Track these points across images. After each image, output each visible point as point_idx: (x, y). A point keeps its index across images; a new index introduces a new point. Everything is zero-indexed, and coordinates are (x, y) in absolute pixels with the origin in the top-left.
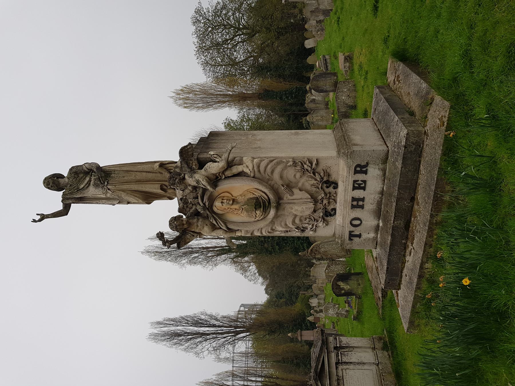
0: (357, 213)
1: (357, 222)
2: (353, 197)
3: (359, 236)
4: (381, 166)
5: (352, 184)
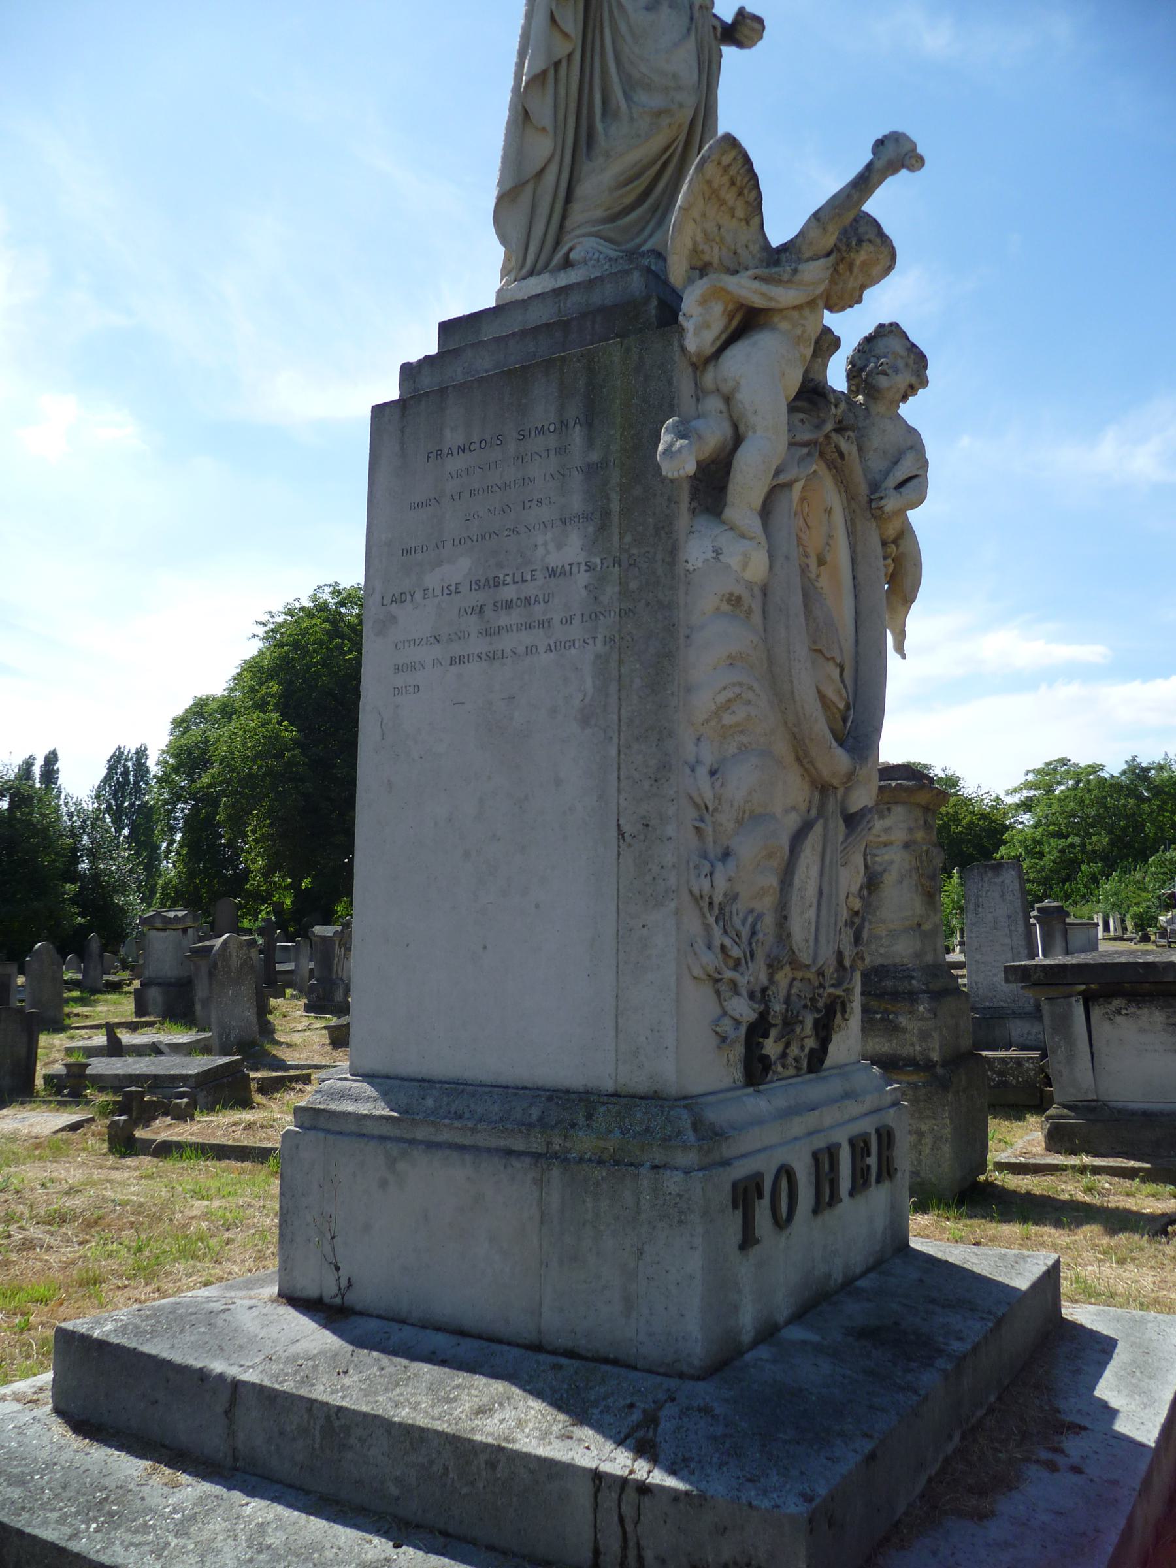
3: (748, 1241)
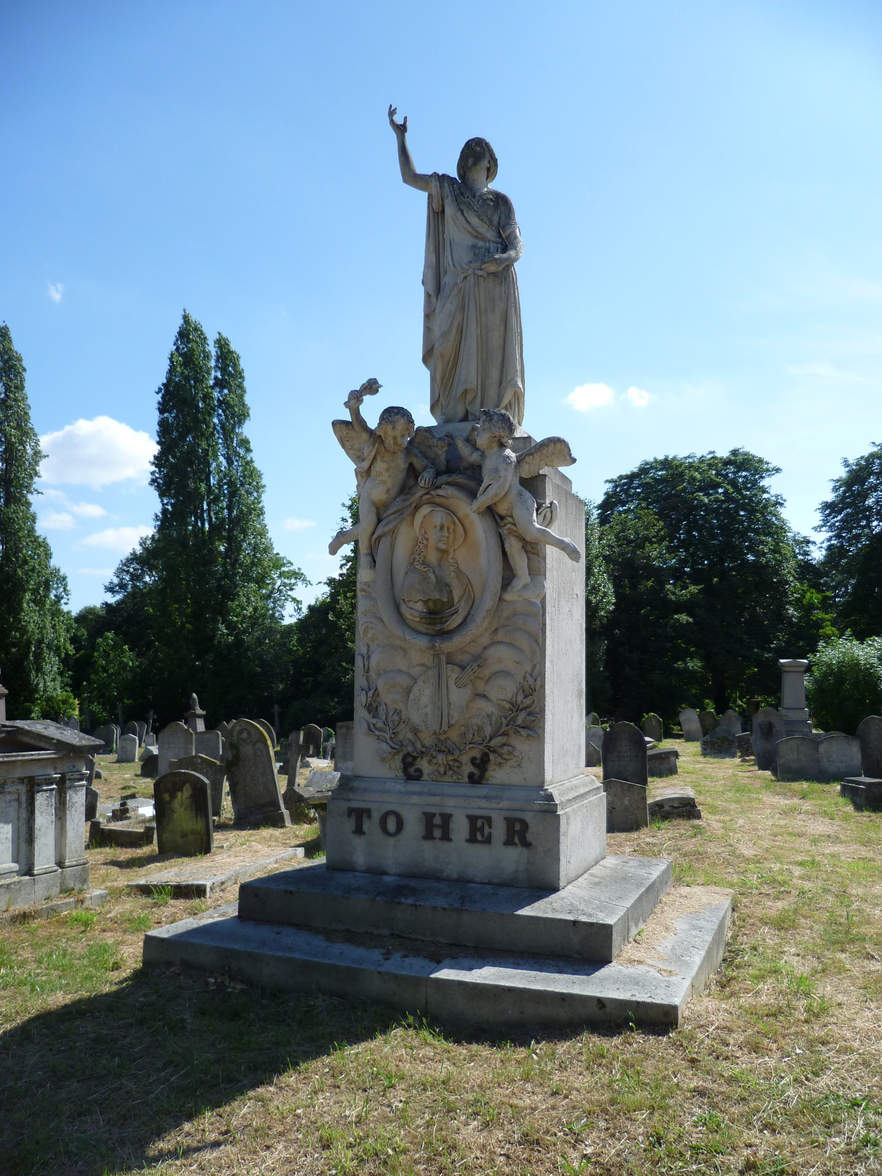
0: (413, 826)
1: (391, 825)
2: (451, 816)
3: (359, 831)
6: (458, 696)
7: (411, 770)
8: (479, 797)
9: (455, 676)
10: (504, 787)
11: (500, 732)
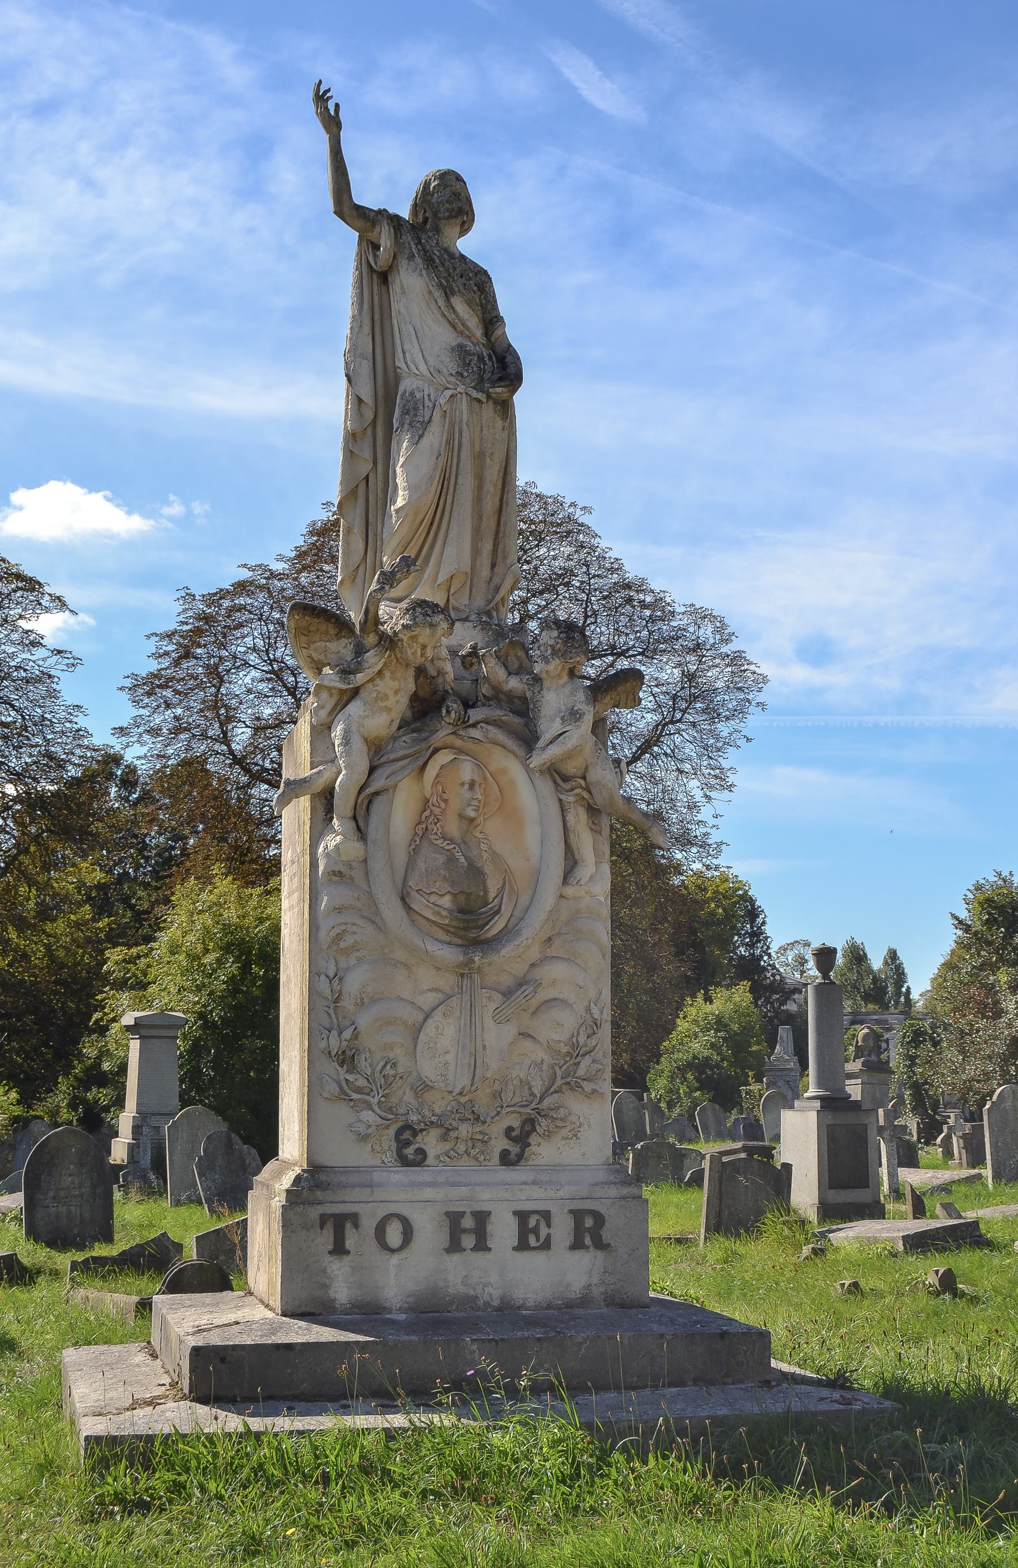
0: (429, 1230)
1: (394, 1235)
2: (489, 1213)
4: (597, 1292)
5: (536, 1208)
6: (496, 1036)
7: (409, 1151)
8: (525, 1183)
9: (492, 1006)
10: (556, 1168)
11: (552, 1090)
